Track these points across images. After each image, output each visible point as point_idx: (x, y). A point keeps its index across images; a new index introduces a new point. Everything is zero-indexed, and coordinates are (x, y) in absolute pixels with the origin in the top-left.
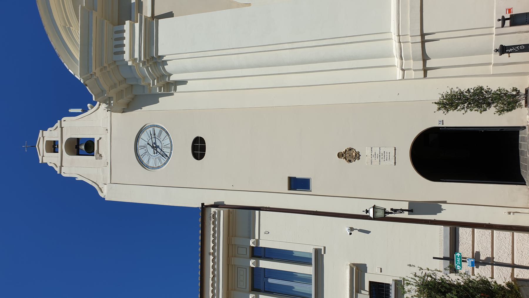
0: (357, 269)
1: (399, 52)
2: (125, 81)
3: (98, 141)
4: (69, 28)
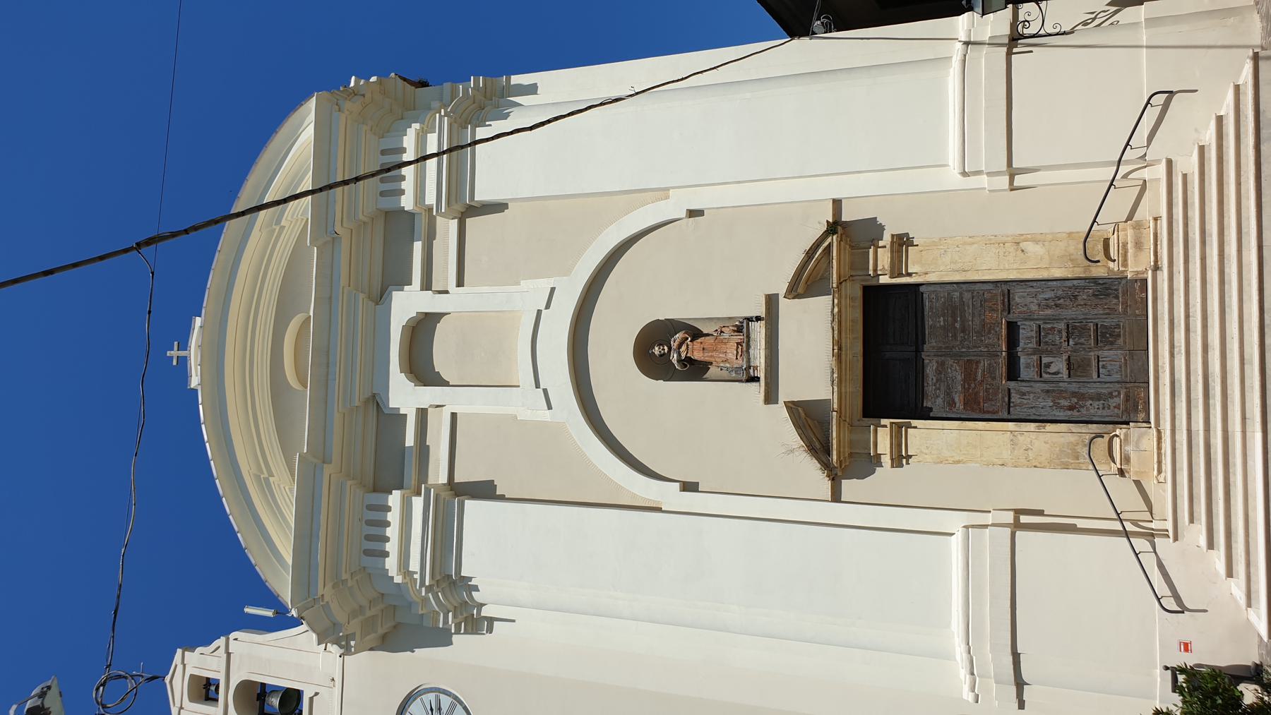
2: (382, 598)
3: (311, 699)
4: (267, 480)
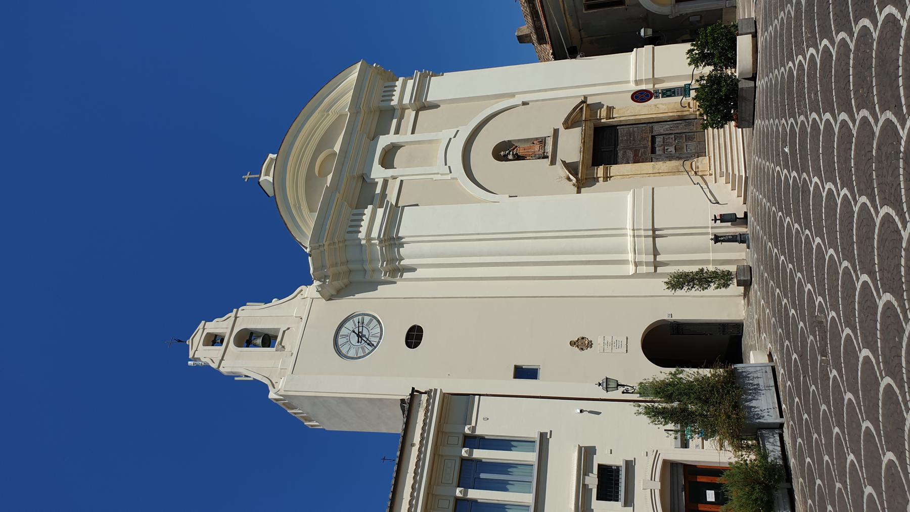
0: (585, 451)
1: (633, 245)
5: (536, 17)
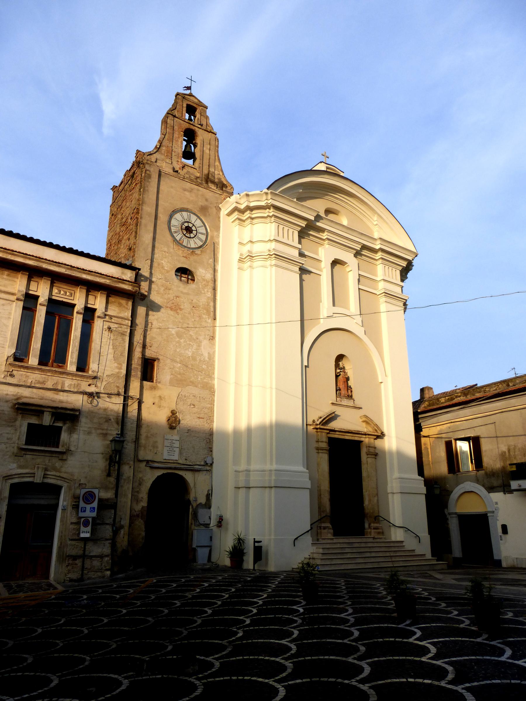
5: (448, 398)
